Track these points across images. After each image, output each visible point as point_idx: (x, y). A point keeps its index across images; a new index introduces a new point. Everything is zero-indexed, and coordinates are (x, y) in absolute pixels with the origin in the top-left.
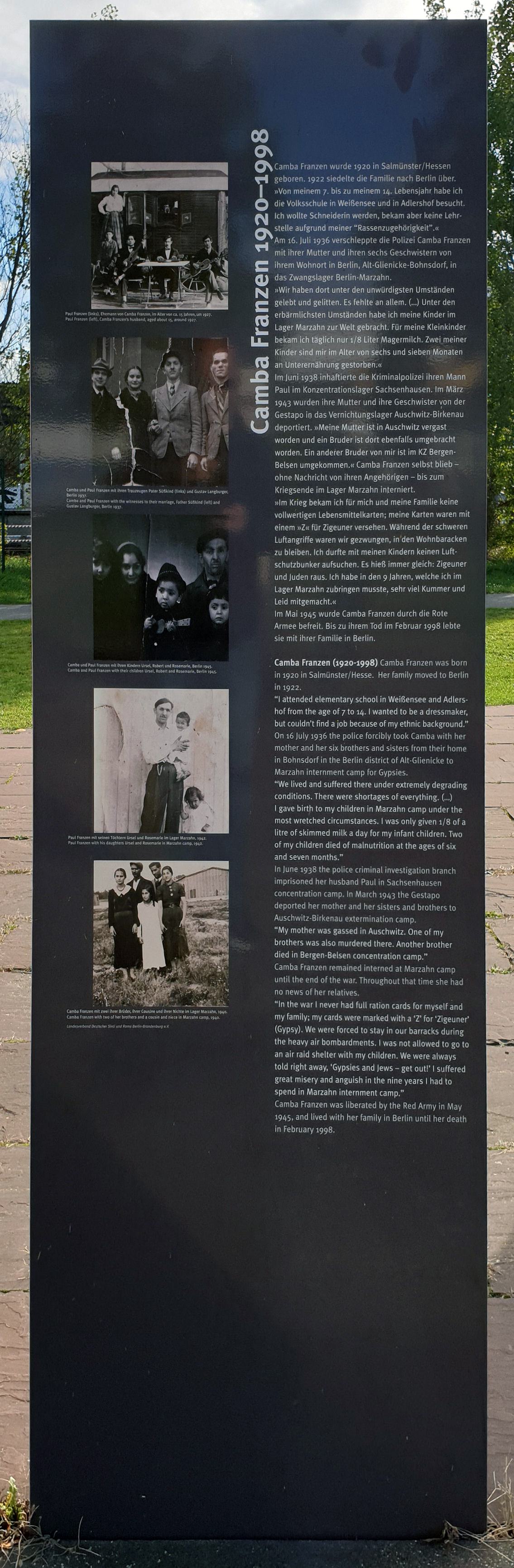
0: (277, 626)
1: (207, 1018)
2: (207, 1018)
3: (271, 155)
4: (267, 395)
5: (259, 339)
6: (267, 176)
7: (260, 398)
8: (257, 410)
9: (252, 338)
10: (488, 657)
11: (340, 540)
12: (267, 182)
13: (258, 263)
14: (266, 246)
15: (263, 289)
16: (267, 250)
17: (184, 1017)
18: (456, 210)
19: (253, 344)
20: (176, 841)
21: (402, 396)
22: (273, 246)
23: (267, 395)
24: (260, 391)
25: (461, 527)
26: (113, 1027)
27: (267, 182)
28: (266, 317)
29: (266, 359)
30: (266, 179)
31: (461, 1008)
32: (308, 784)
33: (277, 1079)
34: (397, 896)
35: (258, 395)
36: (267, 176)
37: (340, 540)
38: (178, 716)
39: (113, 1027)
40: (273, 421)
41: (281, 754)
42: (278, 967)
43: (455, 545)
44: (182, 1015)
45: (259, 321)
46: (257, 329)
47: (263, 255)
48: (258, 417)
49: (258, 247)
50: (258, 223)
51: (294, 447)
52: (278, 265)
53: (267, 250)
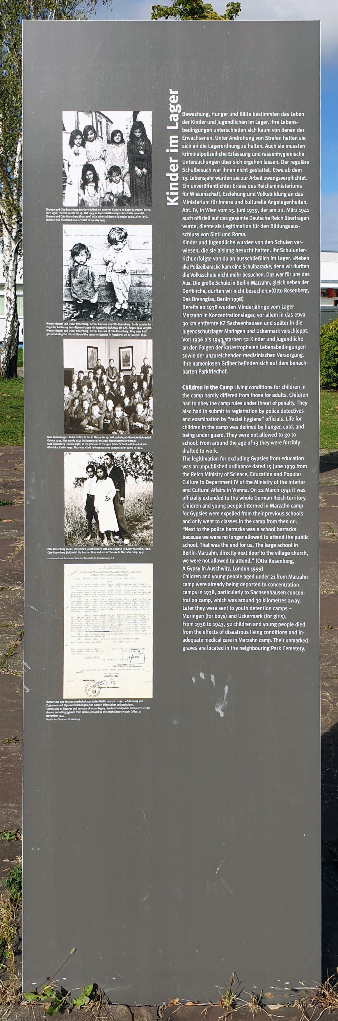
0: (184, 283)
1: (137, 552)
2: (137, 552)
7: (173, 144)
8: (171, 116)
11: (227, 291)
13: (171, 137)
15: (175, 105)
17: (122, 552)
20: (130, 212)
23: (177, 141)
24: (173, 139)
26: (78, 558)
32: (210, 530)
33: (184, 648)
34: (259, 443)
35: (171, 141)
37: (227, 291)
38: (126, 234)
39: (78, 558)
40: (181, 198)
41: (187, 510)
42: (184, 482)
44: (120, 551)
48: (171, 120)
51: (194, 239)
52: (185, 162)
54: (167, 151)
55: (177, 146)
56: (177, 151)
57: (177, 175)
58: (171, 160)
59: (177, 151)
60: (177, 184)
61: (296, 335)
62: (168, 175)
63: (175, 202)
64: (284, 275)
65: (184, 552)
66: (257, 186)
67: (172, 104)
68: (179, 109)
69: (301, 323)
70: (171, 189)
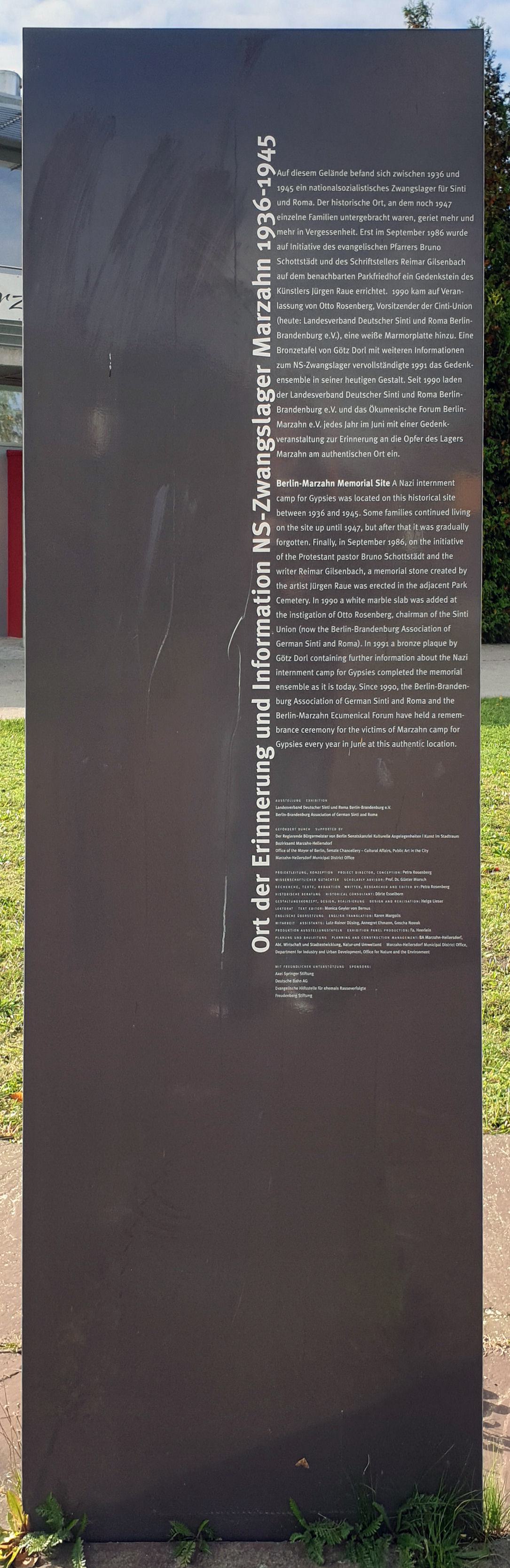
3: (274, 236)
4: (269, 268)
5: (260, 858)
6: (269, 242)
7: (262, 631)
8: (259, 326)
9: (254, 857)
10: (485, 1162)
12: (269, 185)
13: (259, 564)
14: (268, 245)
15: (266, 389)
16: (269, 248)
18: (449, 737)
19: (254, 863)
21: (392, 403)
22: (274, 242)
24: (262, 624)
25: (457, 351)
27: (269, 185)
28: (268, 325)
29: (267, 701)
30: (268, 182)
31: (457, 175)
35: (260, 628)
36: (269, 242)
43: (451, 694)
45: (261, 294)
46: (259, 314)
47: (265, 254)
49: (260, 246)
50: (260, 223)
53: (269, 248)
54: (253, 841)
55: (267, 834)
56: (268, 687)
57: (267, 900)
58: (259, 793)
59: (268, 687)
60: (268, 813)
61: (443, 694)
62: (253, 900)
63: (264, 547)
64: (437, 189)
65: (277, 843)
66: (400, 262)
67: (261, 388)
68: (270, 753)
69: (452, 701)
70: (259, 834)
